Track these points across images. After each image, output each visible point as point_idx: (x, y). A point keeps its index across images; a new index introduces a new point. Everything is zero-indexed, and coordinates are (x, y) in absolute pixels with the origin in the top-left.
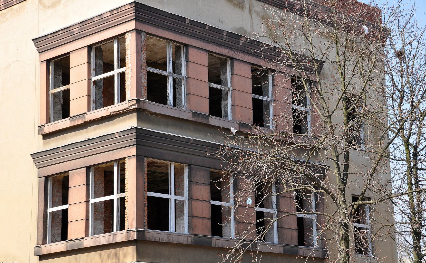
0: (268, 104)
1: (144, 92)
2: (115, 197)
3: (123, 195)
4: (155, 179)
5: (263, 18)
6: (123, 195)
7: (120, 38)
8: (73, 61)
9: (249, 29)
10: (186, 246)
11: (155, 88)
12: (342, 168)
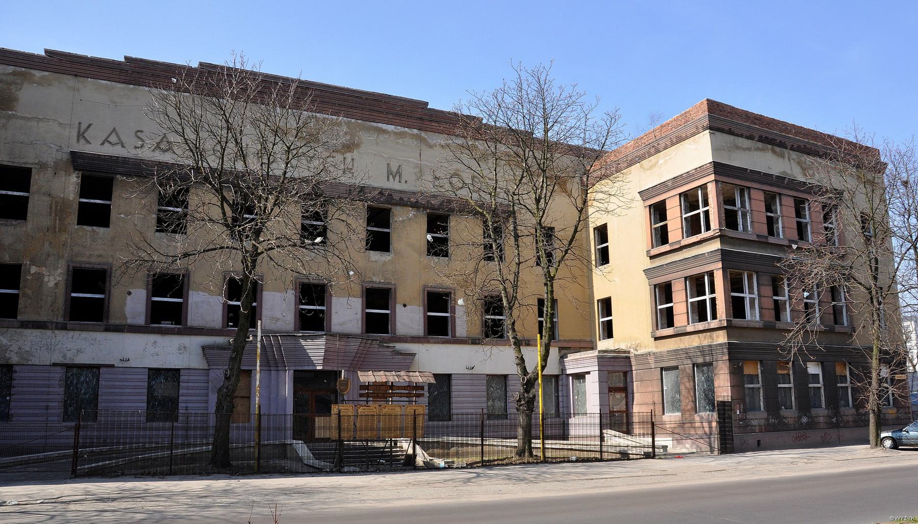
0: (806, 224)
1: (724, 223)
2: (707, 297)
3: (713, 296)
4: (734, 284)
5: (798, 163)
6: (713, 296)
7: (704, 187)
8: (669, 205)
9: (789, 172)
10: (759, 329)
11: (730, 219)
12: (873, 268)
